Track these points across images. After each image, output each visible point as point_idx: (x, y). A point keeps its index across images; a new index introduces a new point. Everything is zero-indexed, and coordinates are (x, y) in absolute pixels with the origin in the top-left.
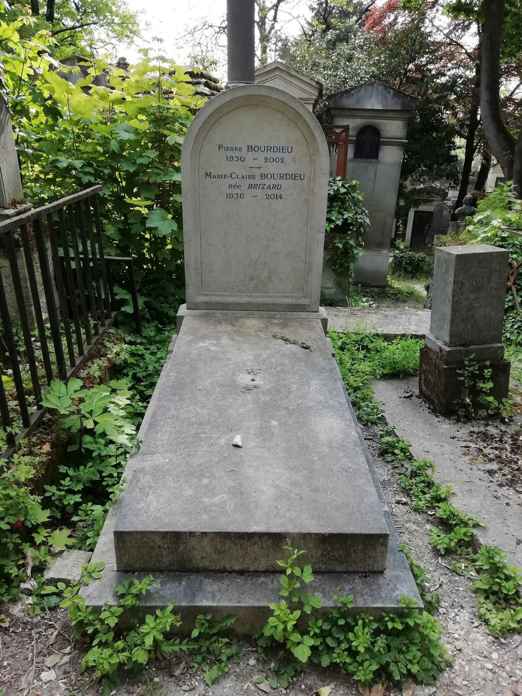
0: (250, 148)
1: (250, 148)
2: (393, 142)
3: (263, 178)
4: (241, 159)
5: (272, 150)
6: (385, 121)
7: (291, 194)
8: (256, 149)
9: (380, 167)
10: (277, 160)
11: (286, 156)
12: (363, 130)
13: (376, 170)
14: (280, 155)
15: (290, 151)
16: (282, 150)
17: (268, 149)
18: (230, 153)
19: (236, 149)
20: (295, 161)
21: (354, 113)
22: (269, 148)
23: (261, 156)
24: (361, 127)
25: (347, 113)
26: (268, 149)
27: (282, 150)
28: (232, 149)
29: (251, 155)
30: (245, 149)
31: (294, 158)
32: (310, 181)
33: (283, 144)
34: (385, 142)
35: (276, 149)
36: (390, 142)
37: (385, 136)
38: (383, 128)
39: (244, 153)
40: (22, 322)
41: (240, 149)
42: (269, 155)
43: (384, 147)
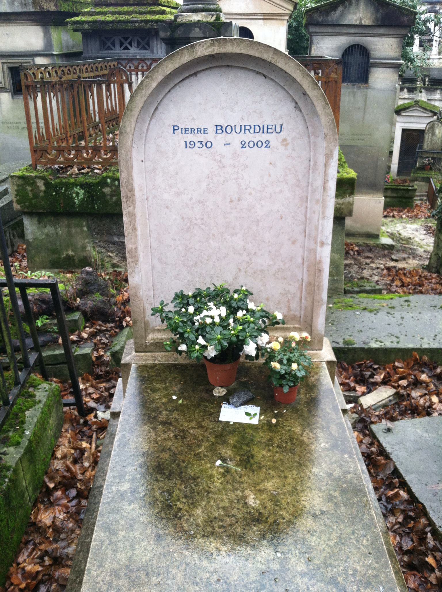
0: (219, 129)
1: (219, 129)
2: (386, 63)
4: (207, 145)
5: (252, 130)
6: (369, 39)
7: (281, 191)
9: (370, 92)
10: (260, 144)
11: (272, 137)
12: (350, 51)
13: (366, 96)
14: (264, 137)
15: (278, 130)
16: (267, 129)
17: (245, 129)
18: (190, 137)
20: (287, 145)
21: (337, 30)
23: (236, 139)
24: (346, 46)
25: (329, 30)
26: (245, 129)
27: (267, 129)
28: (192, 131)
29: (222, 138)
30: (211, 130)
31: (285, 140)
32: (309, 172)
33: (268, 121)
34: (376, 63)
36: (382, 63)
37: (376, 57)
38: (373, 47)
39: (211, 136)
40: (29, 307)
41: (205, 131)
42: (248, 137)
43: (375, 69)
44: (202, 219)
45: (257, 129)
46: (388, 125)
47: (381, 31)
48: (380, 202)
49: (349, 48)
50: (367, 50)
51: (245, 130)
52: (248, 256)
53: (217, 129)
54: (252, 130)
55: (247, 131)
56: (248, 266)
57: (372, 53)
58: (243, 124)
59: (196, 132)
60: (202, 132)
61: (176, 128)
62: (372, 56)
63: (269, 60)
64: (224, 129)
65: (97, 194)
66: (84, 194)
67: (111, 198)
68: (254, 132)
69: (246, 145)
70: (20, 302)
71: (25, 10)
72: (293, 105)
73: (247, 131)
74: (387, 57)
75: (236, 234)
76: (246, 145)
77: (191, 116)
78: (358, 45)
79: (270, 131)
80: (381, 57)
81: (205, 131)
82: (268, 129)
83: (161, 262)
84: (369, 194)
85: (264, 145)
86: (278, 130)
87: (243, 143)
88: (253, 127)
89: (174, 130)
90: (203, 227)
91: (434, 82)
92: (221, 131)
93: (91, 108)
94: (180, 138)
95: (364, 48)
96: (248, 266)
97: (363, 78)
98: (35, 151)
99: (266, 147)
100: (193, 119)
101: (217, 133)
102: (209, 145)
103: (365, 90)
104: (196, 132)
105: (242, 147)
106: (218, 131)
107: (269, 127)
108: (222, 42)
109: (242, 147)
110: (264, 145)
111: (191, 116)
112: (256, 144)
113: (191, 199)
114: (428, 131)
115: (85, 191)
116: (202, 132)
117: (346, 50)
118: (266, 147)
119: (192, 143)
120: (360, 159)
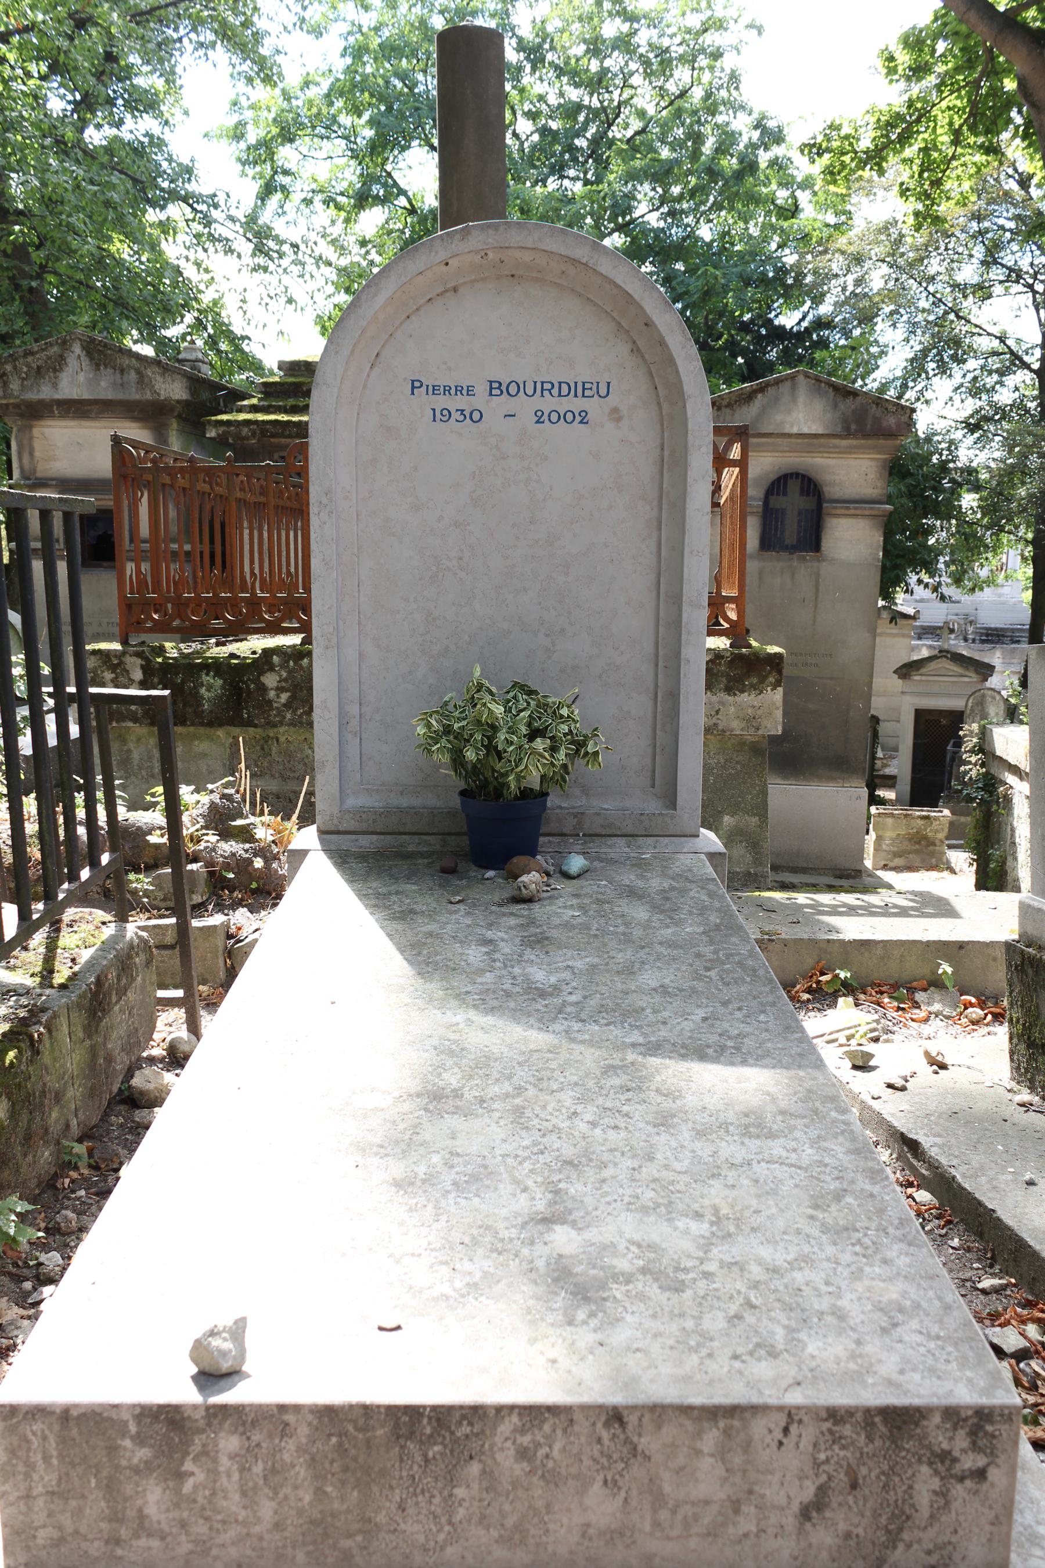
0: (496, 388)
1: (496, 388)
3: (495, 392)
4: (474, 417)
6: (831, 462)
8: (513, 389)
9: (825, 569)
11: (593, 406)
13: (818, 575)
14: (577, 404)
15: (603, 391)
16: (582, 390)
17: (543, 388)
18: (441, 402)
19: (459, 390)
20: (619, 419)
22: (547, 386)
23: (525, 406)
26: (543, 388)
27: (582, 390)
28: (447, 390)
30: (482, 389)
33: (583, 374)
35: (565, 387)
39: (480, 400)
41: (470, 391)
42: (547, 403)
44: (461, 559)
45: (565, 389)
46: (867, 635)
47: (845, 443)
48: (859, 798)
49: (779, 479)
50: (815, 485)
51: (542, 390)
52: (547, 635)
53: (491, 388)
54: (555, 392)
55: (546, 393)
56: (549, 658)
57: (826, 489)
58: (539, 380)
59: (453, 391)
60: (465, 392)
61: (417, 384)
62: (827, 496)
63: (584, 261)
64: (504, 388)
65: (248, 686)
66: (223, 687)
67: (278, 696)
68: (560, 395)
69: (545, 417)
70: (81, 831)
71: (120, 396)
72: (629, 346)
73: (546, 393)
74: (858, 497)
75: (525, 590)
76: (545, 417)
77: (445, 363)
78: (797, 475)
79: (587, 393)
80: (846, 497)
81: (470, 391)
82: (584, 389)
83: (379, 646)
84: (833, 779)
85: (578, 419)
86: (603, 391)
87: (539, 414)
88: (556, 386)
89: (413, 387)
90: (462, 574)
91: (987, 635)
92: (498, 392)
93: (247, 569)
94: (424, 402)
95: (810, 480)
96: (549, 658)
97: (811, 540)
98: (129, 606)
99: (581, 422)
100: (449, 369)
101: (491, 394)
102: (476, 416)
103: (815, 564)
104: (453, 391)
105: (538, 422)
106: (494, 392)
107: (587, 386)
108: (502, 229)
109: (538, 422)
110: (578, 419)
111: (445, 363)
112: (562, 417)
113: (440, 518)
114: (972, 710)
115: (225, 680)
116: (465, 392)
117: (773, 483)
118: (581, 422)
119: (445, 412)
120: (811, 706)
